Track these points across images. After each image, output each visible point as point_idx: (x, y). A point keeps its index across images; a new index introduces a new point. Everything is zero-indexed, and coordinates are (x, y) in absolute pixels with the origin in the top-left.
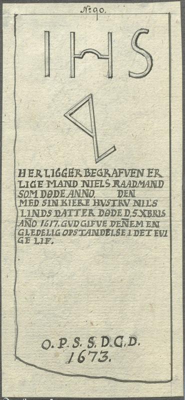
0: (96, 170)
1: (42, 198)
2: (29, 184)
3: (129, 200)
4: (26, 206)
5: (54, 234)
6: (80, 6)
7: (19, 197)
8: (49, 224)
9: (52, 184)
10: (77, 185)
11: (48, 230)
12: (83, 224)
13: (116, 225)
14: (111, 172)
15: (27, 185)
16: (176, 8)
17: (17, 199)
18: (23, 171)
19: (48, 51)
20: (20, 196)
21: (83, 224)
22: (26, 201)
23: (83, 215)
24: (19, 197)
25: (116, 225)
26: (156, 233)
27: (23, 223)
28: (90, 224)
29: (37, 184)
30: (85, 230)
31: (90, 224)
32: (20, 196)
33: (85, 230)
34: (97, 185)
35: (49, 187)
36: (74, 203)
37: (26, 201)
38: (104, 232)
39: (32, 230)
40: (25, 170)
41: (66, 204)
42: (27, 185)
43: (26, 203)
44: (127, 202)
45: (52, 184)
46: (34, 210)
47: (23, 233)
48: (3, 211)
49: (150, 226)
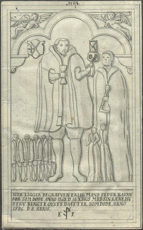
6: (67, 2)
23: (59, 215)
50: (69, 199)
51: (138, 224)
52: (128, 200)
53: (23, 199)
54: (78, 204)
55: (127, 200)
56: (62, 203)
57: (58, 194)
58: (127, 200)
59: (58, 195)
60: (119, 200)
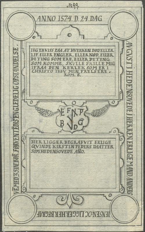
2: (49, 142)
3: (66, 70)
7: (31, 64)
9: (108, 64)
10: (77, 128)
11: (43, 53)
13: (92, 60)
15: (48, 142)
17: (31, 66)
18: (131, 73)
19: (22, 59)
20: (32, 64)
24: (31, 64)
25: (92, 60)
26: (40, 55)
29: (56, 142)
32: (32, 64)
34: (41, 51)
39: (47, 53)
41: (84, 51)
42: (48, 142)
44: (65, 71)
45: (108, 64)
50: (93, 50)
52: (74, 51)
55: (128, 119)
58: (127, 74)
60: (57, 213)
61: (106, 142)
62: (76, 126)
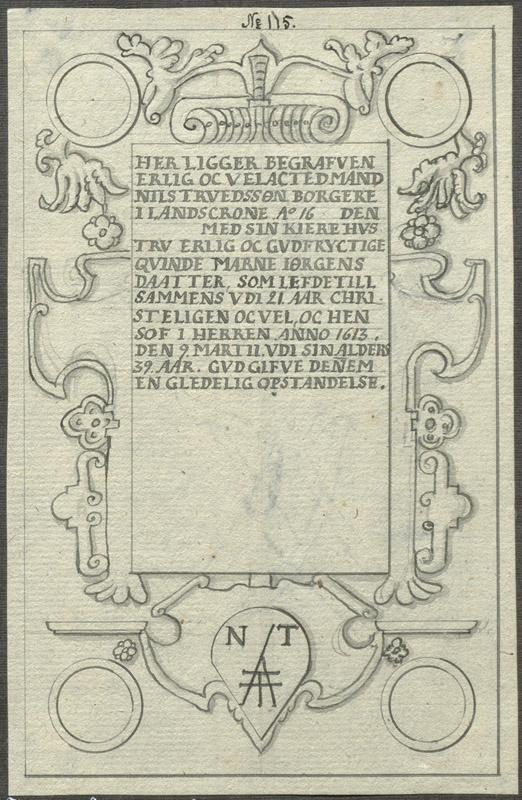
0: (287, 157)
1: (268, 171)
4: (185, 302)
5: (241, 386)
8: (352, 335)
12: (254, 368)
14: (314, 162)
16: (503, 17)
21: (254, 368)
22: (215, 225)
27: (178, 367)
28: (268, 368)
30: (302, 378)
31: (268, 368)
33: (302, 378)
35: (203, 233)
36: (211, 334)
37: (215, 225)
38: (244, 384)
40: (148, 158)
43: (185, 297)
46: (256, 258)
47: (175, 384)
48: (11, 705)
49: (327, 371)
51: (511, 785)
53: (169, 198)
54: (140, 245)
56: (174, 192)
57: (329, 158)
59: (329, 163)
61: (335, 194)
62: (237, 228)
